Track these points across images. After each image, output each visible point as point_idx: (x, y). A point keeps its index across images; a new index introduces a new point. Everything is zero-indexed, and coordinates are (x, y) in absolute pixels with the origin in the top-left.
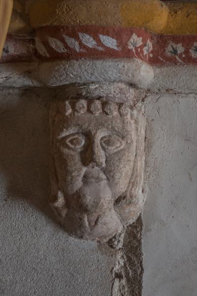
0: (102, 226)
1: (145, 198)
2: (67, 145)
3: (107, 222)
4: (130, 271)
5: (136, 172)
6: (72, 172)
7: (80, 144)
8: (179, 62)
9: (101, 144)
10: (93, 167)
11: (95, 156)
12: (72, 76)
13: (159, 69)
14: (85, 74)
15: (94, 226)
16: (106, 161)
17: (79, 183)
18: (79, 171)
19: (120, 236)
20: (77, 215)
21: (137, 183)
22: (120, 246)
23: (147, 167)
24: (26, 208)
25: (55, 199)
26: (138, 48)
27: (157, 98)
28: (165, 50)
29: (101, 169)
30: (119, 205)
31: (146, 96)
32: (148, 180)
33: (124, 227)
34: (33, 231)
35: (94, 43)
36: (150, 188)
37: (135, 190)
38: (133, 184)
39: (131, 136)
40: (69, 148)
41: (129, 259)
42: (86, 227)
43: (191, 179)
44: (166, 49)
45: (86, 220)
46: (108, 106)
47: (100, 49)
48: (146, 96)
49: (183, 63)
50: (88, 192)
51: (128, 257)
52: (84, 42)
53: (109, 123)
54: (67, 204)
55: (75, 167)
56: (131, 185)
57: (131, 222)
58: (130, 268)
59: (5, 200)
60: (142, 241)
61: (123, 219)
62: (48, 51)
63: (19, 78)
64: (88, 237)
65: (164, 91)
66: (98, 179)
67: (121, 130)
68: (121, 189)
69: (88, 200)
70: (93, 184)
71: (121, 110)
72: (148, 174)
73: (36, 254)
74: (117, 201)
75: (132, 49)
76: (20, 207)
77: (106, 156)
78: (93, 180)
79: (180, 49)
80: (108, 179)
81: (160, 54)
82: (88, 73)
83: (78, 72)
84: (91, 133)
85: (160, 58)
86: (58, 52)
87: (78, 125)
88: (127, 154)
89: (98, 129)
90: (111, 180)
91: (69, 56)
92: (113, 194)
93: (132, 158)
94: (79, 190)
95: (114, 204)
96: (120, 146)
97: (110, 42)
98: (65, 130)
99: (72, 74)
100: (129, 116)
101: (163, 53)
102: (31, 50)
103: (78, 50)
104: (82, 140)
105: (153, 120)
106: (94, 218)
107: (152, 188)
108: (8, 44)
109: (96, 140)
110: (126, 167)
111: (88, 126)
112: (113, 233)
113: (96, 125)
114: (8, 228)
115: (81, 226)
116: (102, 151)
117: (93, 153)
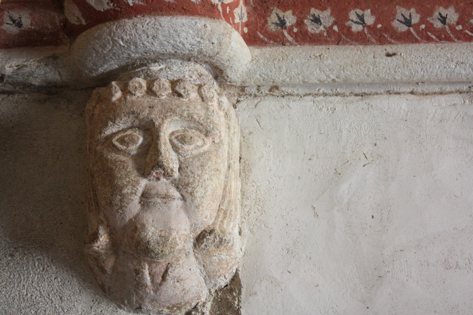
0: (174, 283)
1: (244, 246)
2: (114, 146)
3: (183, 276)
5: (228, 194)
6: (122, 188)
8: (288, 41)
9: (171, 141)
10: (158, 179)
11: (160, 158)
12: (121, 43)
13: (259, 50)
14: (143, 39)
15: (160, 284)
16: (180, 169)
17: (134, 206)
19: (204, 306)
20: (131, 266)
21: (230, 214)
23: (244, 200)
24: (46, 266)
25: (95, 237)
27: (256, 102)
28: (266, 22)
29: (172, 182)
30: (203, 246)
31: (238, 101)
32: (247, 217)
33: (210, 292)
34: (57, 302)
36: (252, 231)
37: (228, 224)
38: (225, 213)
39: (220, 132)
40: (118, 151)
42: (146, 286)
43: (316, 215)
44: (268, 19)
45: (146, 272)
48: (238, 101)
49: (294, 43)
50: (150, 221)
54: (114, 246)
55: (127, 179)
56: (221, 215)
57: (223, 282)
59: (12, 255)
61: (209, 277)
62: (84, 15)
63: (38, 66)
64: (150, 308)
65: (265, 90)
66: (166, 197)
68: (206, 217)
69: (150, 234)
70: (158, 206)
71: (202, 90)
72: (246, 210)
74: (200, 239)
76: (36, 265)
77: (179, 160)
78: (159, 200)
79: (290, 19)
80: (184, 199)
81: (259, 29)
82: (148, 37)
84: (154, 124)
85: (259, 34)
86: (100, 11)
87: (133, 113)
88: (214, 158)
90: (189, 200)
94: (135, 217)
95: (195, 246)
96: (202, 146)
98: (110, 123)
99: (123, 40)
100: (215, 104)
101: (264, 25)
102: (57, 22)
104: (139, 136)
105: (250, 133)
106: (160, 269)
107: (255, 230)
108: (22, 14)
109: (162, 134)
110: (214, 178)
111: (148, 114)
112: (192, 300)
113: (162, 112)
115: (139, 284)
117: (157, 152)
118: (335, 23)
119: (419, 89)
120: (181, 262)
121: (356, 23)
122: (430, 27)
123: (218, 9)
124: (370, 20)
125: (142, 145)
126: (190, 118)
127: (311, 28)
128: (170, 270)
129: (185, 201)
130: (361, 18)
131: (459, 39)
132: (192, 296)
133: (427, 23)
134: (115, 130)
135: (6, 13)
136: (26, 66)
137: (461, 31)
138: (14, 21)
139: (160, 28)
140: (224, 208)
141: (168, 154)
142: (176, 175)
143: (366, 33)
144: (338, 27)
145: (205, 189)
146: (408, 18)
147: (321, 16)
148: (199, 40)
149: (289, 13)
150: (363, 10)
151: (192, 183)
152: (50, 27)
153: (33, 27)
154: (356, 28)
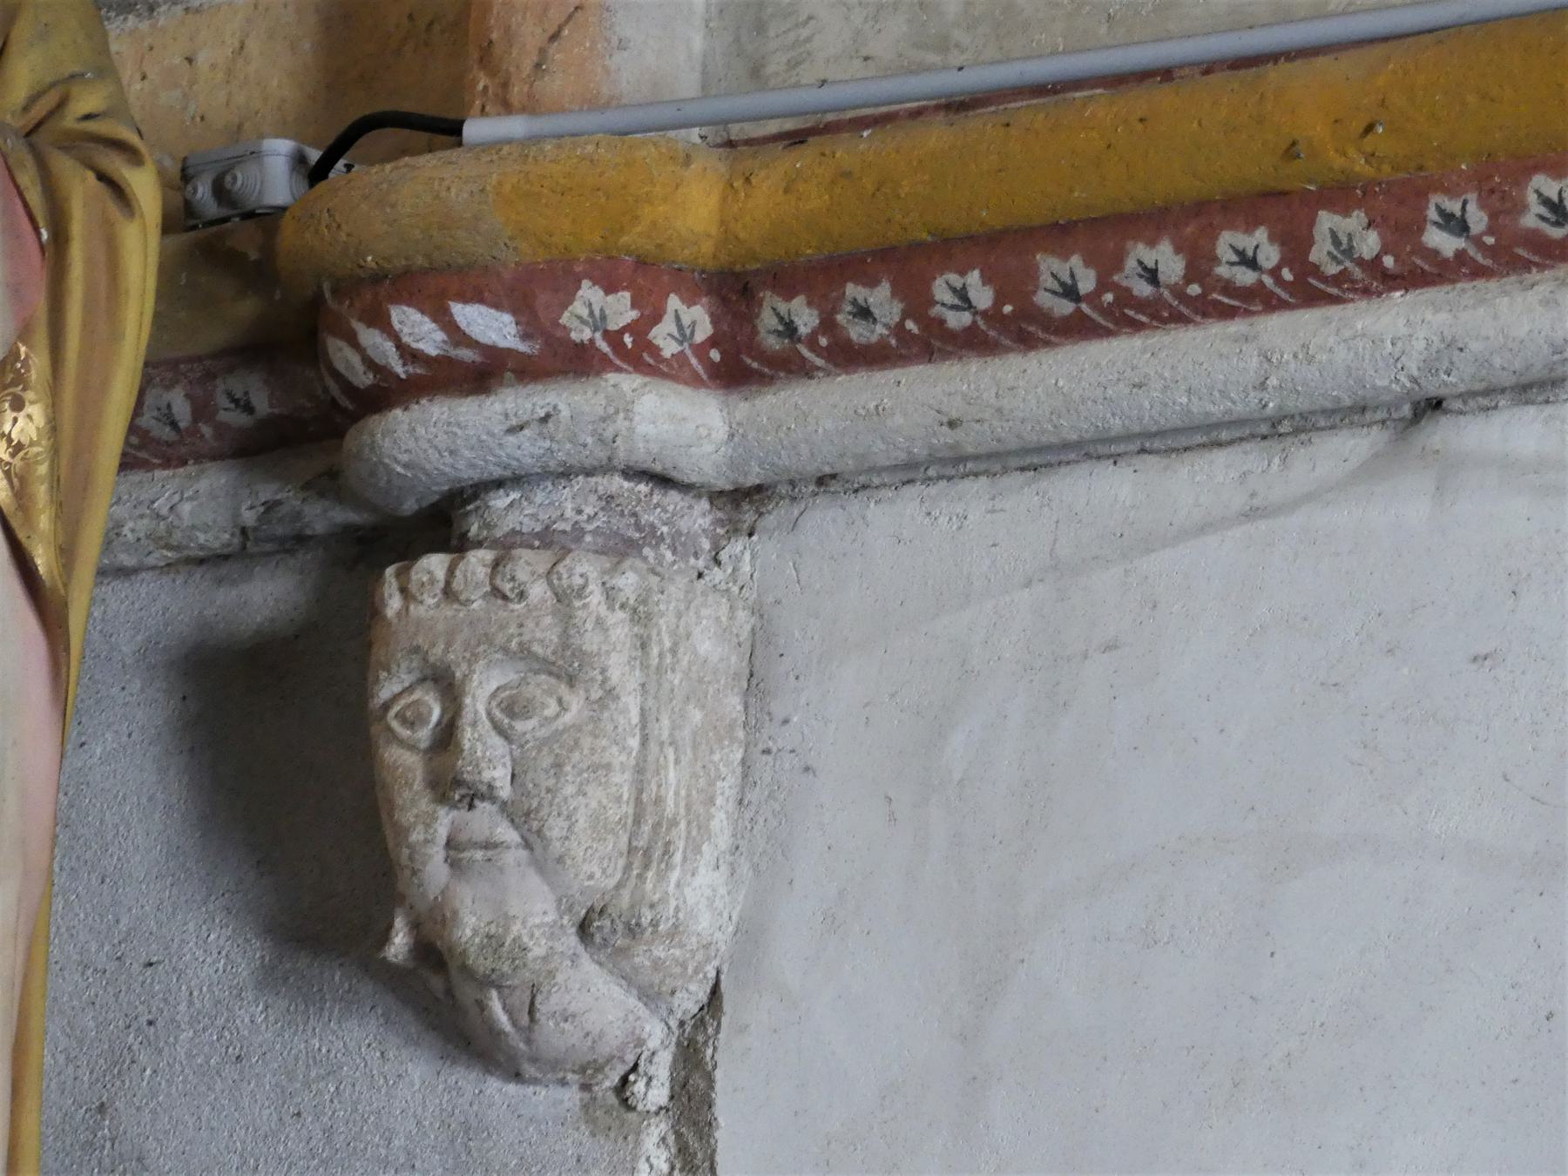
0: (557, 1024)
1: (739, 908)
8: (818, 368)
9: (489, 714)
15: (530, 1029)
17: (436, 870)
18: (428, 828)
22: (658, 1094)
25: (385, 938)
26: (622, 331)
32: (747, 835)
35: (440, 336)
36: (756, 868)
37: (661, 877)
38: (647, 853)
41: (683, 1150)
42: (506, 1035)
43: (892, 818)
46: (509, 567)
47: (466, 354)
51: (679, 1135)
52: (406, 339)
53: (513, 630)
55: (415, 811)
60: (718, 1074)
67: (554, 653)
68: (591, 877)
72: (748, 815)
73: (383, 1152)
75: (592, 341)
78: (479, 855)
80: (527, 845)
83: (426, 441)
85: (749, 361)
88: (587, 742)
89: (475, 656)
91: (385, 394)
92: (559, 901)
93: (623, 755)
94: (443, 892)
96: (558, 716)
97: (491, 326)
100: (595, 598)
103: (399, 369)
106: (521, 999)
110: (589, 789)
112: (622, 1048)
114: (297, 1059)
116: (496, 740)
118: (906, 315)
119: (1157, 444)
120: (560, 978)
121: (953, 307)
122: (1126, 297)
123: (598, 350)
124: (983, 297)
125: (439, 723)
126: (525, 653)
127: (858, 332)
128: (539, 998)
129: (532, 849)
130: (962, 294)
131: (1205, 315)
132: (615, 1043)
133: (1116, 287)
134: (397, 688)
135: (219, 381)
136: (278, 503)
137: (1203, 296)
138: (236, 401)
139: (459, 432)
141: (479, 747)
142: (505, 792)
143: (983, 327)
144: (916, 321)
145: (569, 817)
146: (1069, 282)
147: (871, 300)
148: (547, 444)
149: (799, 303)
150: (963, 273)
151: (537, 810)
152: (308, 405)
153: (276, 411)
154: (958, 320)
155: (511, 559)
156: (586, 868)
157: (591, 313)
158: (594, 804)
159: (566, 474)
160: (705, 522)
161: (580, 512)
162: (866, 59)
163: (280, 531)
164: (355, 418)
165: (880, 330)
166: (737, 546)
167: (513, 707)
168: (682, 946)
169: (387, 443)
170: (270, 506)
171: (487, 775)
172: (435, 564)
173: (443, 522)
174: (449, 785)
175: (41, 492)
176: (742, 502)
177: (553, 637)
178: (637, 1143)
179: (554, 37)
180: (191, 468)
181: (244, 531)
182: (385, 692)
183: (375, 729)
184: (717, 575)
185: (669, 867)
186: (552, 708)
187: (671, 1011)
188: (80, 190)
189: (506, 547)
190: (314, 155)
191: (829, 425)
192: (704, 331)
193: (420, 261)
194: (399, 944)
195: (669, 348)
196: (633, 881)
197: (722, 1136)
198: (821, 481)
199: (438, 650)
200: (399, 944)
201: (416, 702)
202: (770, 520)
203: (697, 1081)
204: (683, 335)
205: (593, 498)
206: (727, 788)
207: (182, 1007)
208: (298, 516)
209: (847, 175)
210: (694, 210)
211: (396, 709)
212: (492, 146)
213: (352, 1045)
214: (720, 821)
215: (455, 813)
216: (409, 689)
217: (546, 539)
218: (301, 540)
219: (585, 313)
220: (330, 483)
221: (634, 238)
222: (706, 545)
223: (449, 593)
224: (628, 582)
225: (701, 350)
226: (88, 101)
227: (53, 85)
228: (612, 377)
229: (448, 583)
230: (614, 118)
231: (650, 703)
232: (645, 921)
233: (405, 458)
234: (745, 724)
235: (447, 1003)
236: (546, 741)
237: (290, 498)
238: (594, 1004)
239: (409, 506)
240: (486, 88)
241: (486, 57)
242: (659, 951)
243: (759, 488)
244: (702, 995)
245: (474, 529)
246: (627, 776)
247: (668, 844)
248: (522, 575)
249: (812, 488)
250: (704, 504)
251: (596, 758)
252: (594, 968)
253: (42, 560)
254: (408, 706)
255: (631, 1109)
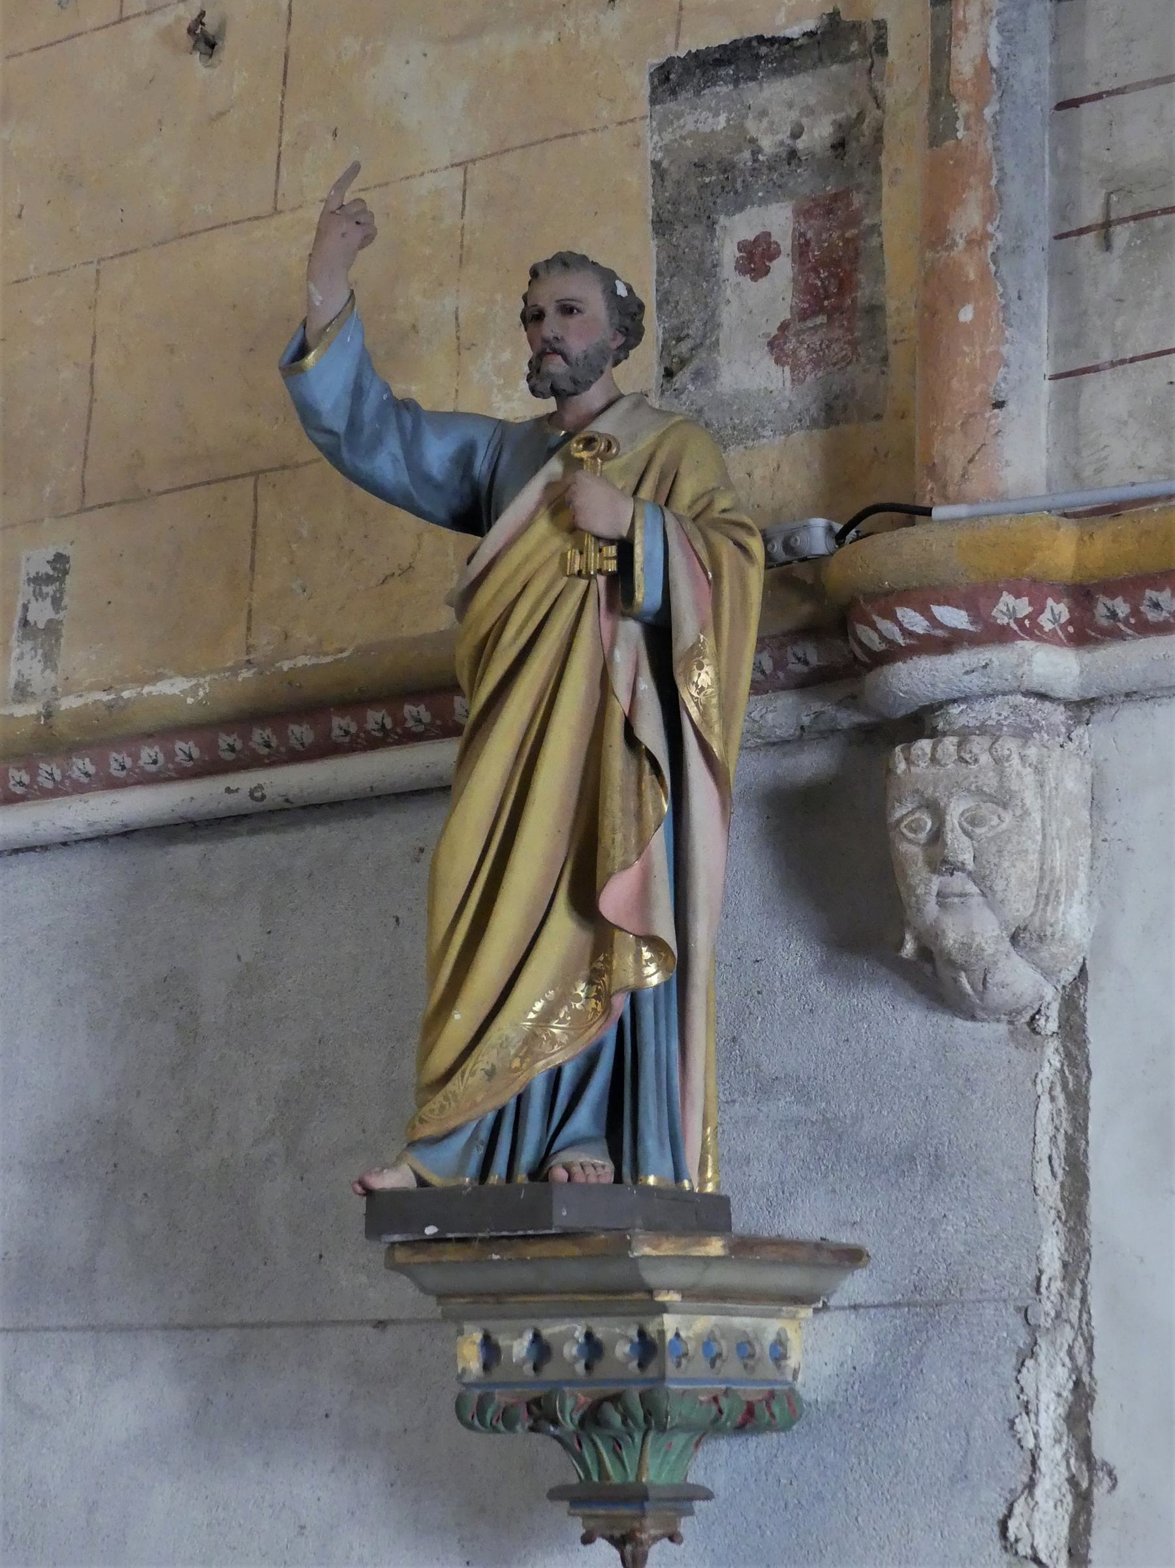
4: (1070, 1078)
7: (923, 829)
9: (960, 824)
17: (931, 908)
18: (928, 888)
22: (1053, 1026)
25: (901, 944)
36: (1102, 903)
37: (1055, 909)
38: (1047, 897)
41: (1068, 1055)
47: (939, 633)
56: (1042, 900)
58: (1071, 1073)
60: (1088, 1015)
68: (1018, 911)
78: (956, 900)
80: (983, 894)
83: (915, 679)
88: (1015, 838)
91: (892, 654)
93: (1033, 847)
97: (954, 617)
100: (1015, 760)
103: (901, 641)
110: (1017, 864)
114: (844, 1010)
116: (965, 838)
120: (1000, 965)
126: (980, 791)
127: (1152, 616)
128: (989, 976)
132: (1029, 999)
135: (789, 649)
136: (823, 713)
138: (799, 659)
140: (1043, 892)
142: (970, 866)
149: (1119, 600)
155: (969, 741)
156: (1016, 906)
157: (1008, 610)
158: (1020, 872)
159: (992, 695)
160: (1062, 718)
161: (1000, 715)
162: (1140, 467)
163: (822, 727)
164: (869, 668)
165: (1165, 614)
166: (1080, 731)
167: (974, 821)
168: (1066, 946)
169: (894, 681)
170: (818, 715)
171: (961, 858)
172: (925, 745)
173: (920, 722)
174: (941, 863)
175: (714, 713)
176: (1083, 707)
177: (994, 783)
178: (1043, 1052)
179: (971, 461)
180: (771, 695)
181: (802, 728)
182: (898, 813)
183: (892, 834)
184: (1071, 746)
185: (1059, 904)
186: (995, 821)
187: (1059, 981)
188: (726, 550)
189: (964, 736)
190: (838, 527)
191: (1137, 666)
192: (1065, 616)
193: (915, 584)
194: (909, 948)
195: (1048, 627)
196: (1039, 914)
197: (1093, 1049)
198: (1127, 695)
199: (930, 790)
200: (909, 948)
201: (918, 820)
202: (1098, 717)
203: (1075, 1018)
204: (1055, 620)
205: (1007, 707)
206: (1084, 860)
207: (777, 984)
208: (833, 719)
209: (1147, 533)
210: (1063, 551)
211: (905, 823)
212: (942, 522)
213: (876, 1002)
214: (1082, 878)
215: (941, 878)
216: (912, 812)
217: (982, 730)
218: (833, 731)
219: (1005, 609)
220: (852, 701)
221: (1032, 569)
222: (1063, 730)
223: (934, 760)
224: (1032, 752)
225: (1063, 627)
226: (723, 502)
227: (703, 495)
228: (1020, 643)
229: (933, 755)
230: (1014, 506)
231: (1046, 816)
232: (1048, 933)
233: (906, 688)
234: (1091, 826)
235: (936, 979)
236: (992, 838)
237: (830, 709)
238: (1019, 979)
239: (902, 712)
240: (932, 489)
241: (932, 470)
242: (1054, 949)
243: (1093, 700)
244: (1075, 971)
245: (941, 725)
246: (1036, 855)
247: (1058, 891)
248: (976, 750)
249: (1122, 698)
250: (1062, 708)
251: (1019, 847)
252: (1018, 958)
253: (716, 747)
254: (912, 821)
255: (1039, 1033)
